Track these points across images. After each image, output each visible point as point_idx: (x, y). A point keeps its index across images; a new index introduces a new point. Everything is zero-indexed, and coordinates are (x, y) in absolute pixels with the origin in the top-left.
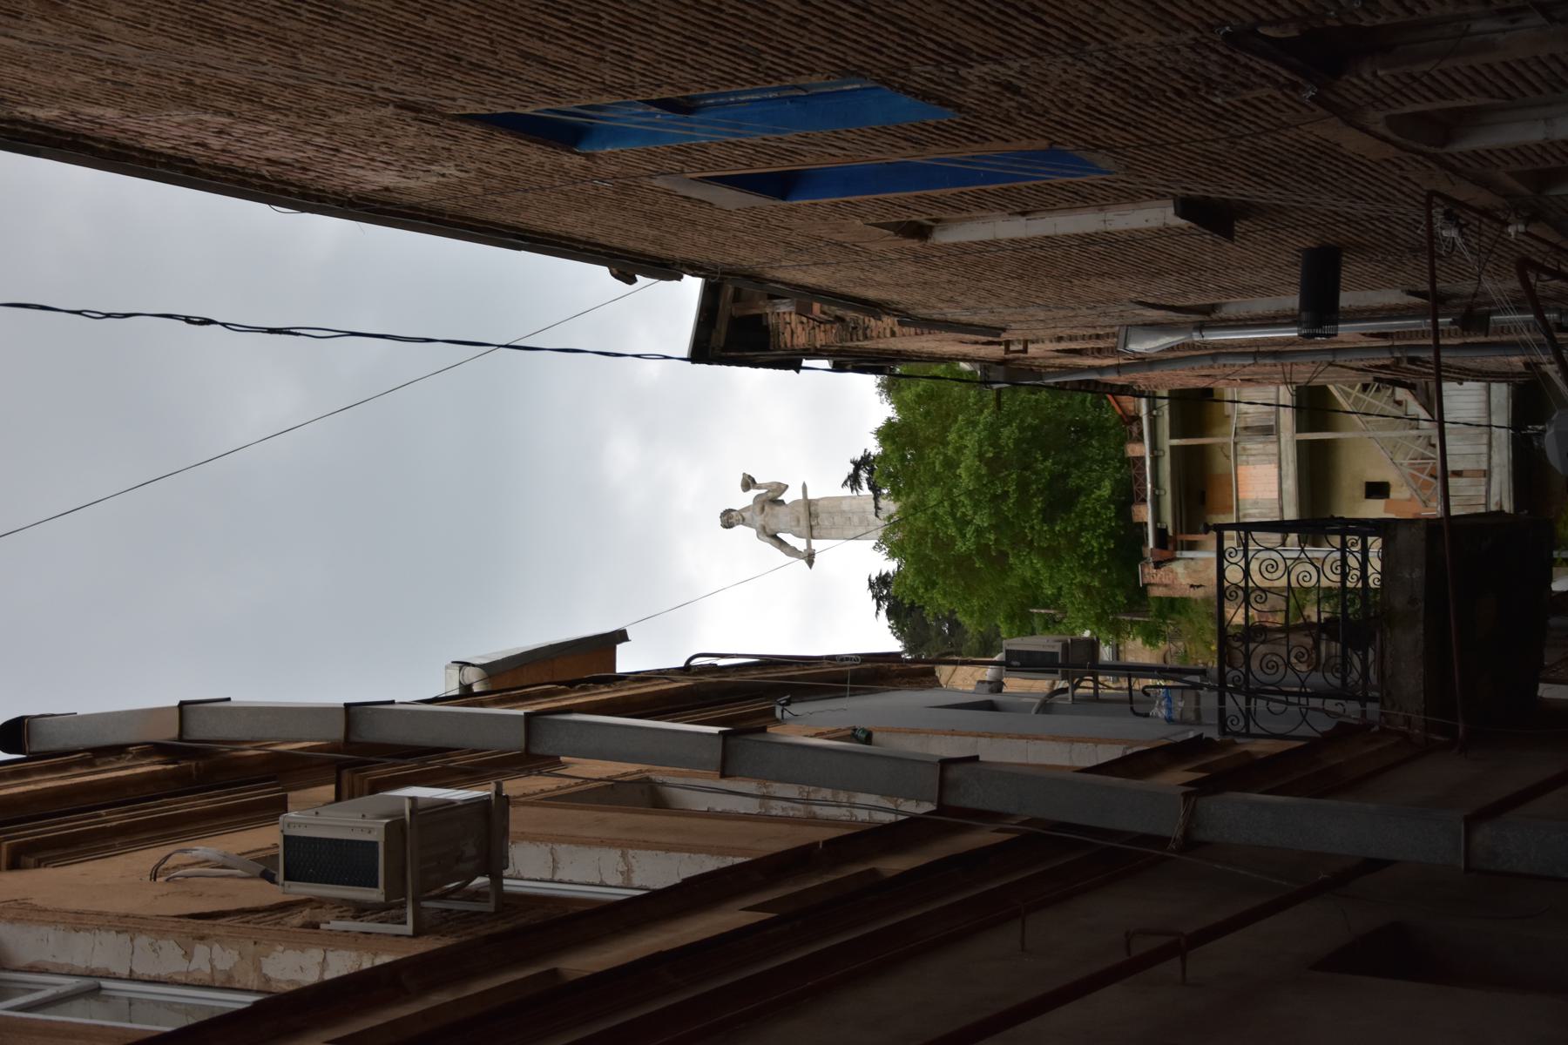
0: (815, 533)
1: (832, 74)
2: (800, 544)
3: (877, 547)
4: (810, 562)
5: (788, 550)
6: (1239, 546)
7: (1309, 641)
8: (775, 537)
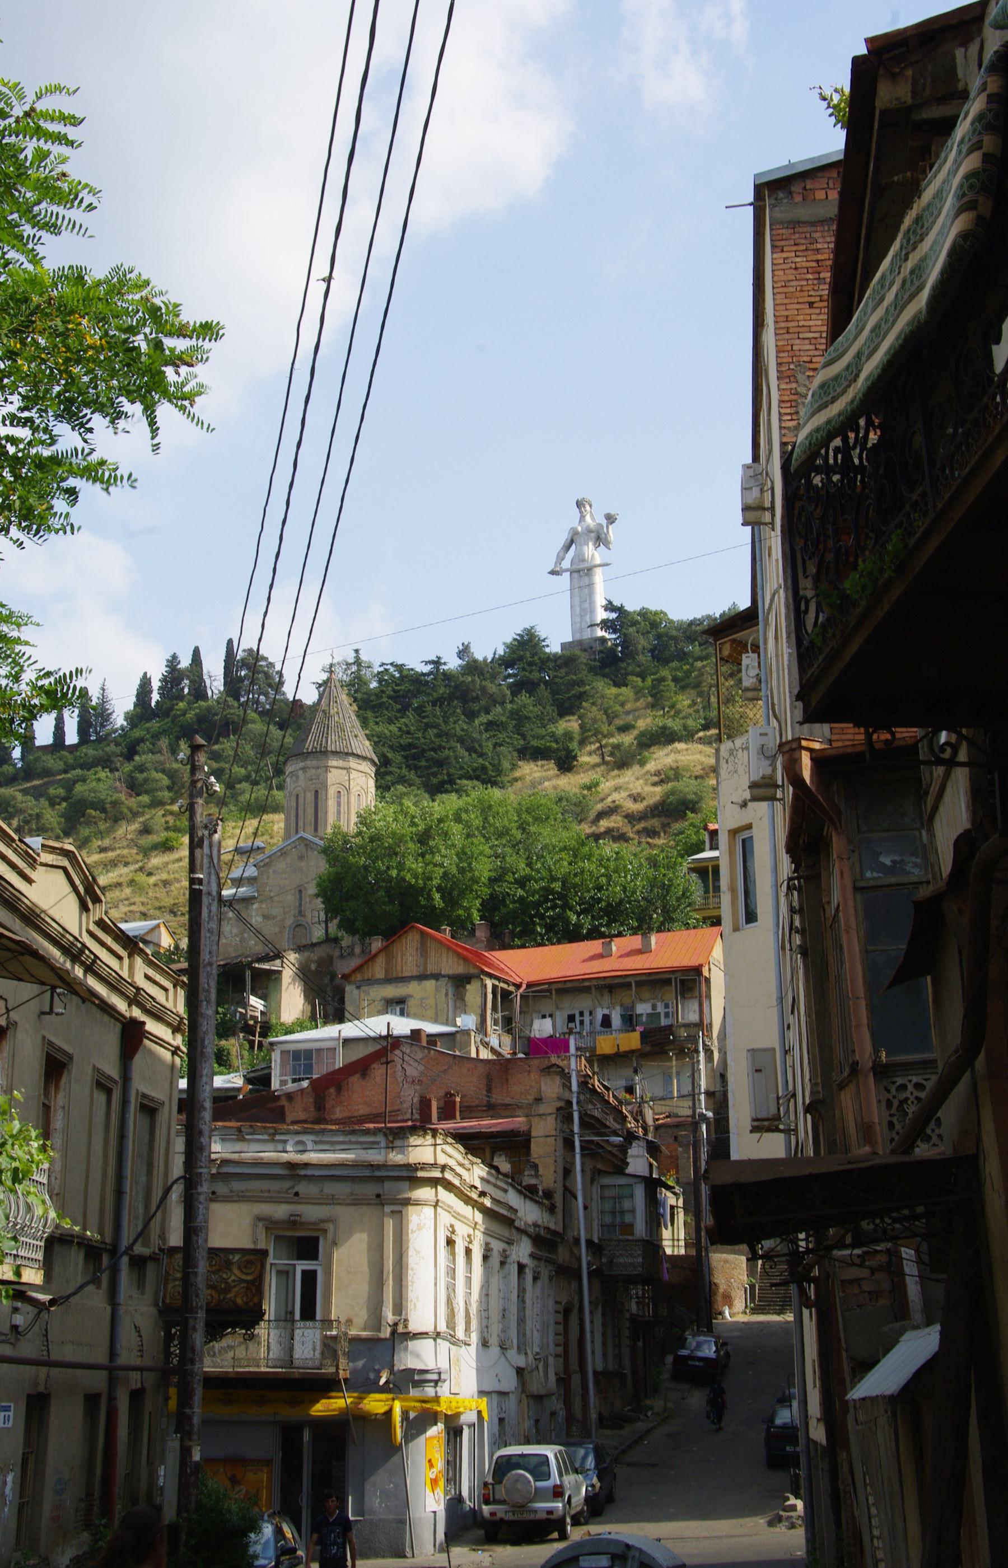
0: (575, 575)
1: (116, 1095)
2: (566, 564)
3: (485, 660)
4: (553, 573)
5: (562, 554)
6: (42, 156)
7: (553, 1142)
8: (572, 542)
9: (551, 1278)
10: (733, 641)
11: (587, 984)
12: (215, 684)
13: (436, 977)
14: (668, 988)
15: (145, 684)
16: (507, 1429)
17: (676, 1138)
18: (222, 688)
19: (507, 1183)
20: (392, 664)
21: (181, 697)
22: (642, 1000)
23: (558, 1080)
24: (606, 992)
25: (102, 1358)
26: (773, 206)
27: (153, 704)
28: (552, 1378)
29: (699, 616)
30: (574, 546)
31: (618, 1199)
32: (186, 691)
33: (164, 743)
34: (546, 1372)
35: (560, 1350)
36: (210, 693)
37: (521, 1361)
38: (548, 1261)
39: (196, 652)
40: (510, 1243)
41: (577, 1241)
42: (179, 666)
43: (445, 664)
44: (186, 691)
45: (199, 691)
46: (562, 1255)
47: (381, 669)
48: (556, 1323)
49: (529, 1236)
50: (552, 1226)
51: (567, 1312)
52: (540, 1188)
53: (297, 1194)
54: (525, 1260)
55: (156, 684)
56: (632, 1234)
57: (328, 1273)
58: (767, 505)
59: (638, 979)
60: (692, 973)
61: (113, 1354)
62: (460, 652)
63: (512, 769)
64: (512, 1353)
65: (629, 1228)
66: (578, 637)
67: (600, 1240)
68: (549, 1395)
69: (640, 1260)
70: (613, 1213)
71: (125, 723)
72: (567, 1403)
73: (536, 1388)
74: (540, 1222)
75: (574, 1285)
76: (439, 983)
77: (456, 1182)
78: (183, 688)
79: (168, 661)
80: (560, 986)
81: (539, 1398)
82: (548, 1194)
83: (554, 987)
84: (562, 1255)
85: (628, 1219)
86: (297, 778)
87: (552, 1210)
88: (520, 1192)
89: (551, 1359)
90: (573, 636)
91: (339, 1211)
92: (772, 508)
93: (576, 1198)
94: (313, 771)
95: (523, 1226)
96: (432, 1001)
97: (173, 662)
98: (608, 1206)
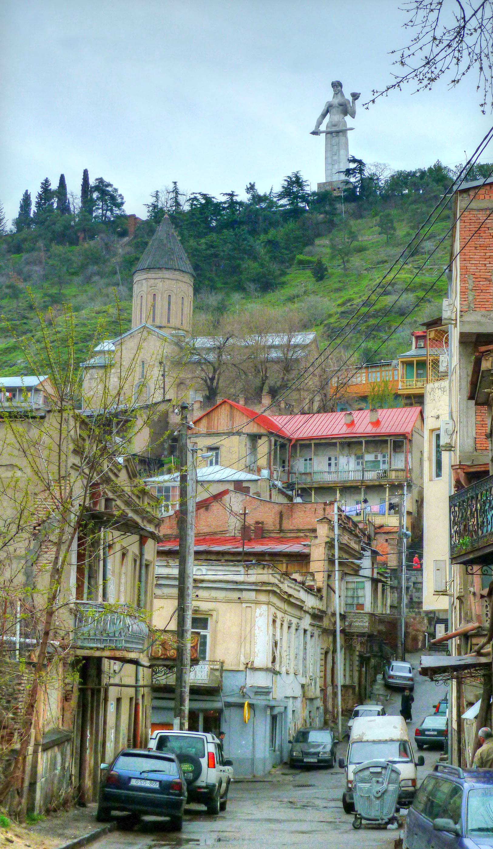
0: (329, 135)
2: (323, 128)
4: (315, 133)
8: (328, 111)
9: (319, 636)
10: (436, 330)
11: (334, 441)
12: (76, 201)
13: (239, 433)
14: (385, 445)
15: (27, 199)
16: (296, 716)
17: (387, 540)
18: (80, 205)
19: (300, 587)
20: (200, 193)
21: (51, 211)
22: (369, 452)
23: (326, 526)
24: (346, 446)
25: (133, 683)
26: (461, 201)
27: (32, 215)
28: (318, 689)
29: (414, 170)
30: (329, 114)
31: (355, 590)
32: (55, 205)
33: (41, 244)
34: (315, 685)
35: (323, 674)
36: (72, 209)
37: (303, 681)
38: (318, 627)
39: (62, 178)
40: (300, 619)
41: (334, 614)
42: (50, 187)
43: (237, 195)
44: (55, 205)
45: (64, 207)
46: (326, 623)
47: (192, 196)
48: (321, 660)
49: (310, 614)
50: (321, 607)
51: (326, 653)
52: (315, 587)
53: (197, 596)
54: (308, 627)
55: (34, 200)
56: (363, 610)
57: (214, 639)
58: (454, 318)
59: (367, 439)
60: (402, 437)
61: (137, 680)
62: (248, 189)
63: (281, 275)
64: (300, 678)
65: (361, 606)
66: (329, 180)
67: (345, 612)
68: (316, 698)
69: (367, 624)
70: (353, 597)
71: (13, 227)
72: (325, 702)
73: (311, 695)
74: (315, 606)
75: (331, 638)
76: (241, 438)
77: (278, 591)
78: (53, 203)
79: (42, 183)
80: (317, 441)
81: (311, 700)
82: (319, 590)
83: (313, 442)
84: (326, 623)
85: (361, 601)
86: (142, 285)
87: (321, 598)
88: (306, 591)
89: (318, 680)
90: (326, 179)
91: (219, 606)
92: (456, 320)
93: (334, 592)
94: (153, 281)
95: (307, 610)
96: (236, 449)
97: (46, 184)
98: (350, 593)
